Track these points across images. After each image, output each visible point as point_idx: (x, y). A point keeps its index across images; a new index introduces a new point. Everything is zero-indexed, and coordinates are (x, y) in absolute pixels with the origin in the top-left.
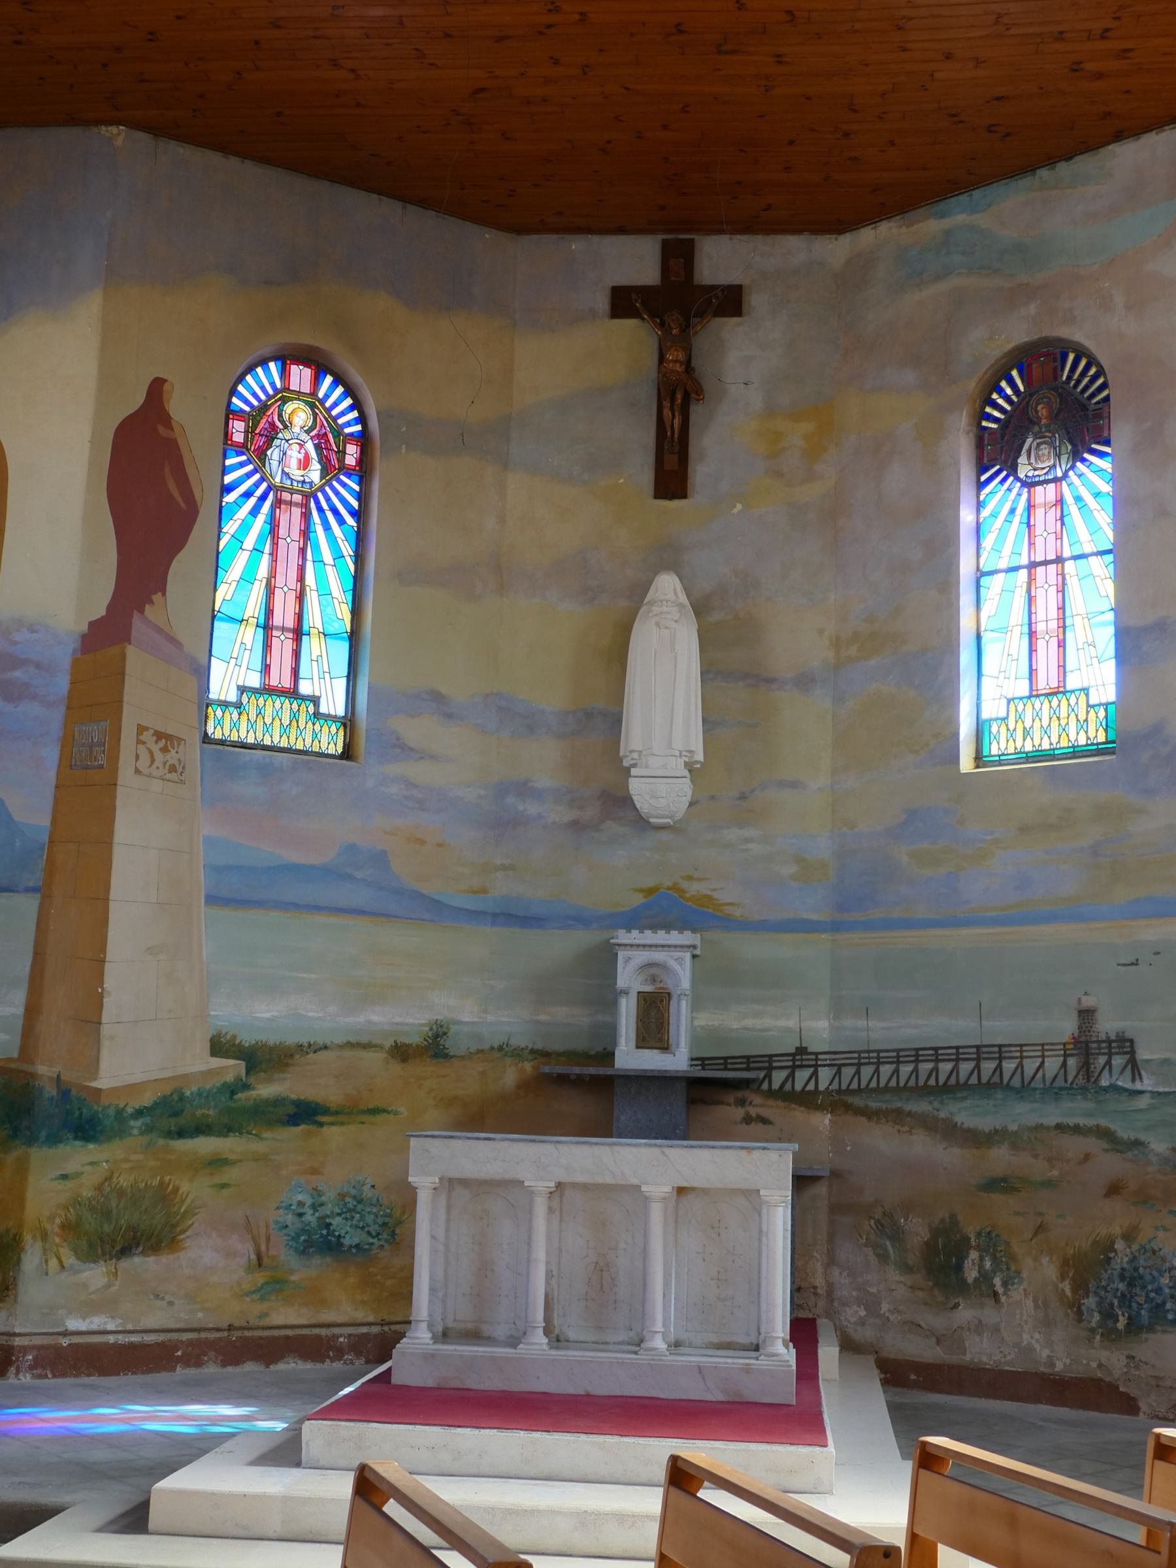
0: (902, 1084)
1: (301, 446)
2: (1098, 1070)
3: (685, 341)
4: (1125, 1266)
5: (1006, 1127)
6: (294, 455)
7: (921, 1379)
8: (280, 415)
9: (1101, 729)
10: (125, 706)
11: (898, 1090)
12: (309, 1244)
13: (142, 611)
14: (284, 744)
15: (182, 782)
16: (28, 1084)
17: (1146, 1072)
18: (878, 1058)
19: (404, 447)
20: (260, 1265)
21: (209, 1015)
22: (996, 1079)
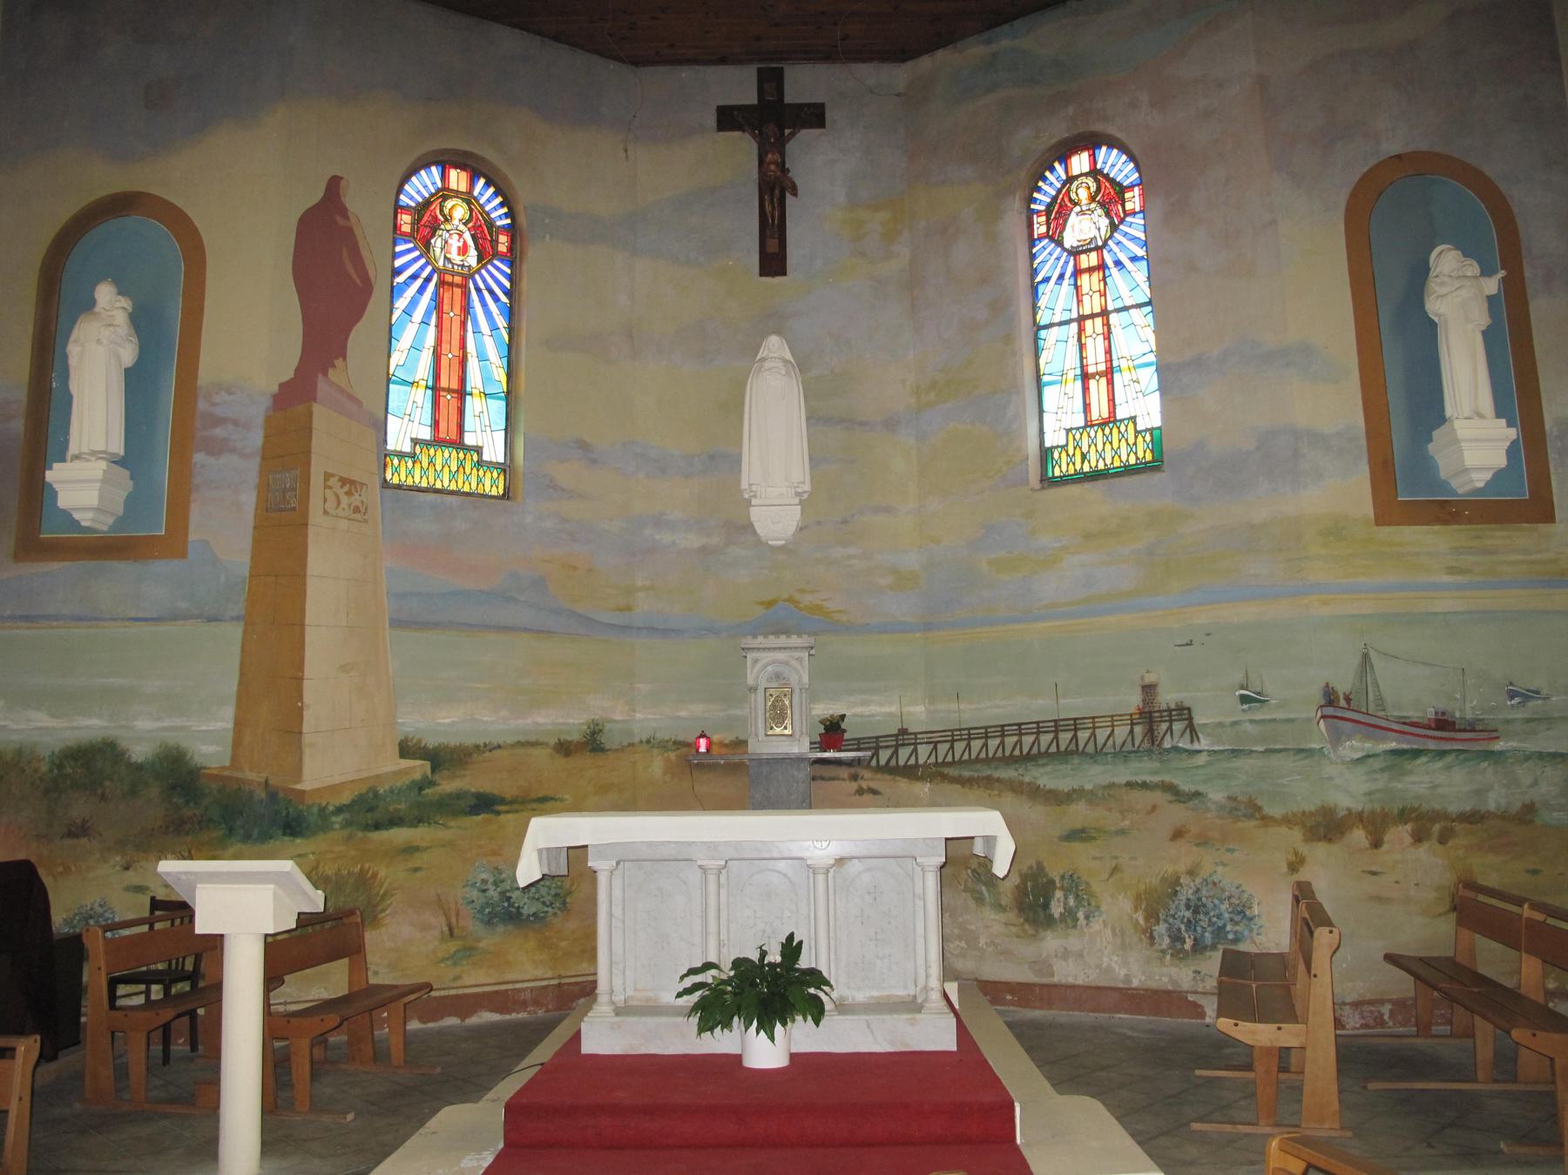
0: (990, 755)
1: (460, 236)
2: (1161, 735)
3: (780, 144)
4: (1191, 897)
5: (1083, 787)
6: (455, 243)
7: (1016, 999)
8: (441, 211)
9: (1148, 450)
10: (313, 456)
11: (988, 761)
12: (493, 915)
13: (325, 374)
14: (453, 487)
15: (366, 521)
16: (240, 789)
17: (1202, 733)
18: (969, 734)
19: (548, 236)
20: (451, 935)
21: (397, 723)
22: (1073, 747)
